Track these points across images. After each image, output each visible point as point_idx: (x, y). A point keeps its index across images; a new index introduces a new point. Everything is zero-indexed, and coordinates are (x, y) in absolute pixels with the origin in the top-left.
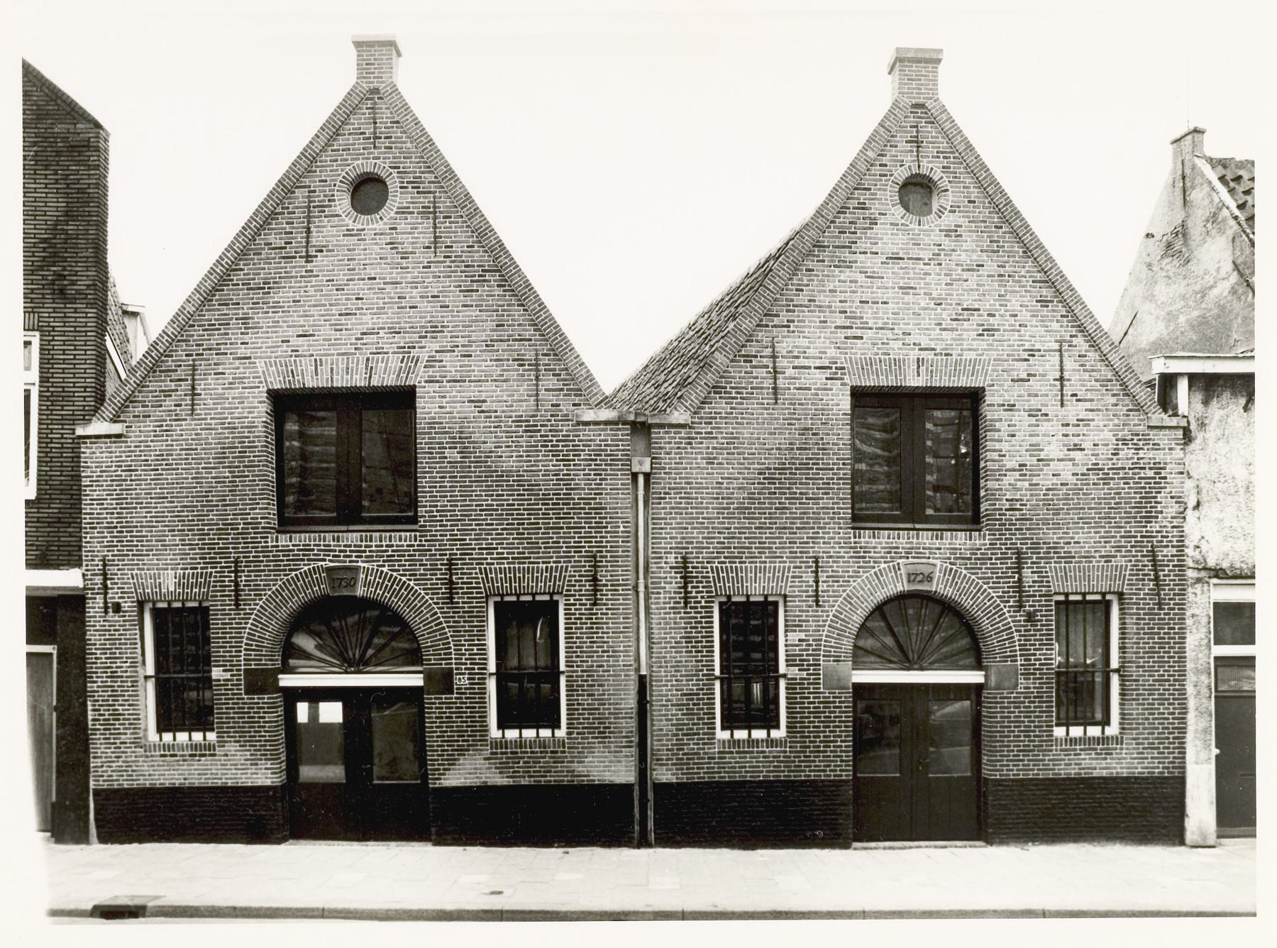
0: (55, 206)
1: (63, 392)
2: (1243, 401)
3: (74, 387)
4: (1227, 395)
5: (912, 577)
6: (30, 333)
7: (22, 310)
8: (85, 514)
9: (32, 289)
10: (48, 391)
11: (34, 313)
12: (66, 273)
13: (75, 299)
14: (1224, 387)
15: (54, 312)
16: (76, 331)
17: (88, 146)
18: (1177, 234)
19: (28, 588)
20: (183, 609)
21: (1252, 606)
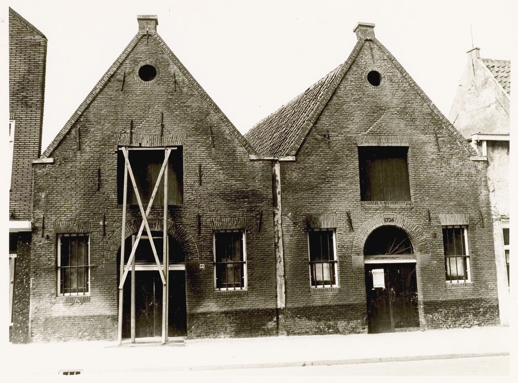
0: (23, 68)
1: (25, 144)
2: (506, 151)
3: (30, 142)
4: (500, 148)
5: (386, 220)
6: (12, 120)
7: (9, 111)
8: (115, 199)
9: (13, 102)
10: (18, 144)
11: (13, 112)
12: (27, 96)
13: (32, 106)
14: (499, 146)
15: (22, 112)
16: (31, 119)
17: (40, 45)
18: (472, 86)
19: (10, 229)
20: (232, 233)
21: (508, 229)
